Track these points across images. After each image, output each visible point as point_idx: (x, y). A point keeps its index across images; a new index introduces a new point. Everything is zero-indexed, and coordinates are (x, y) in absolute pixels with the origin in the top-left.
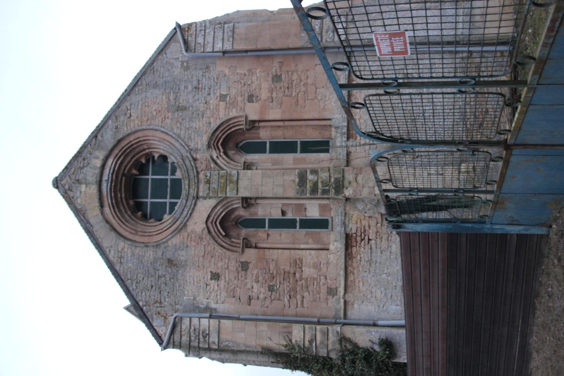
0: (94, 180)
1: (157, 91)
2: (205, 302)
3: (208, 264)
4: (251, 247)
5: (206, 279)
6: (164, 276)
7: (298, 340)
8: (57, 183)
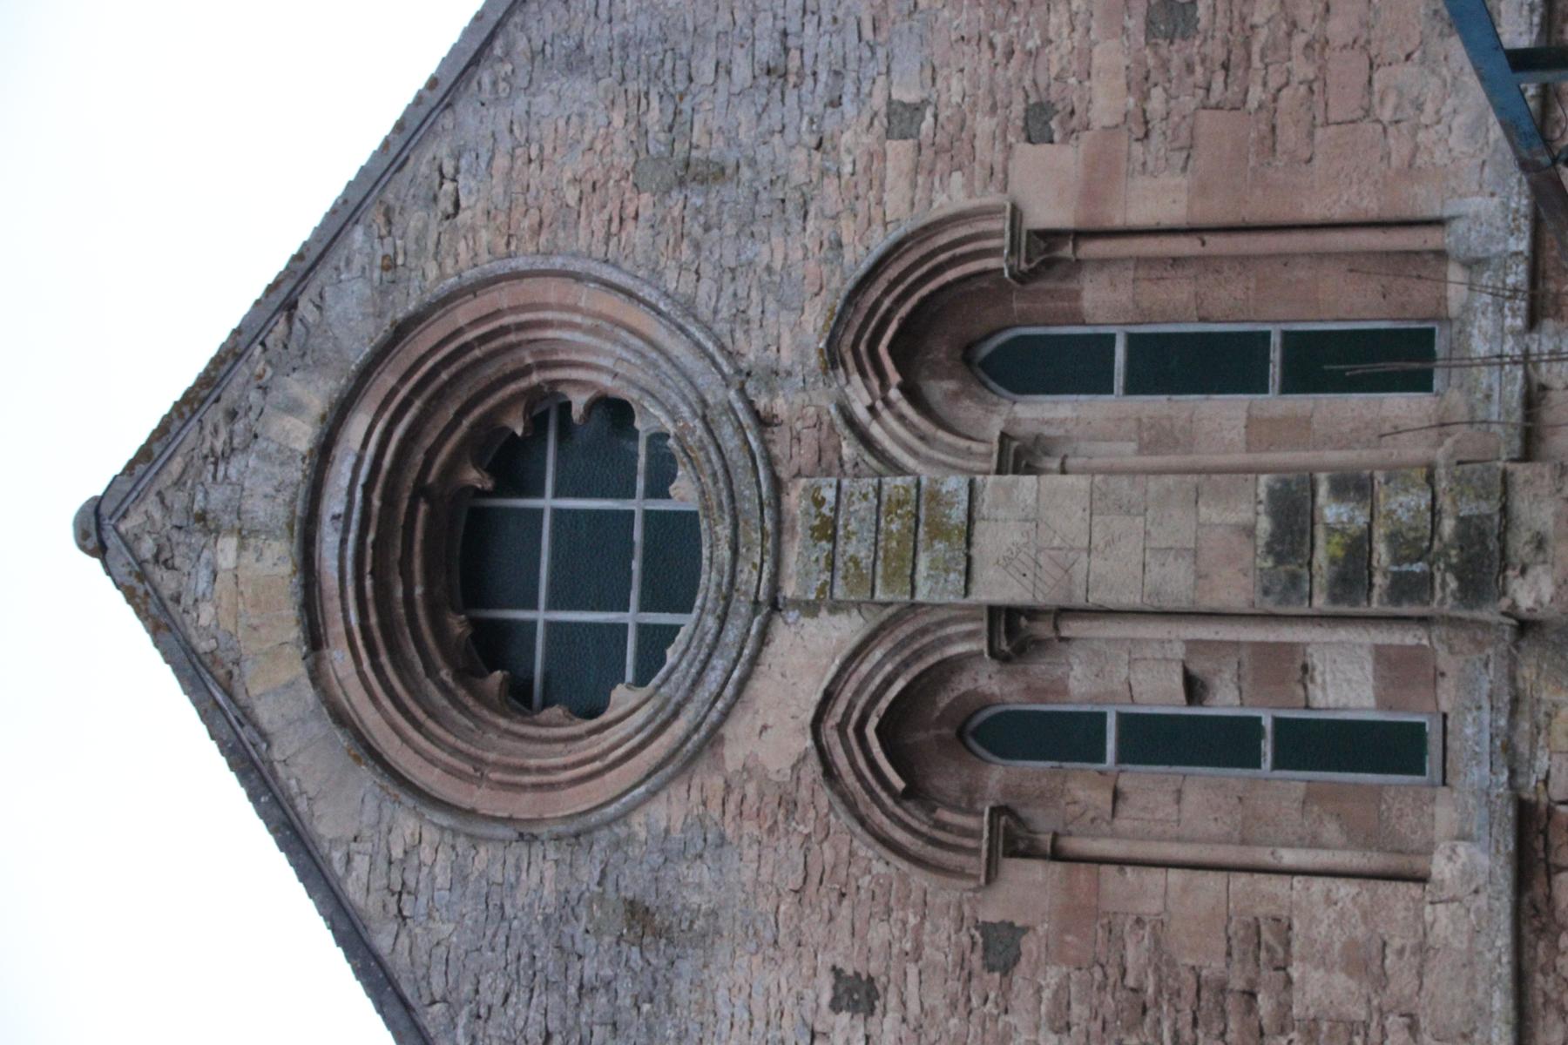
1: (581, 89)
3: (820, 933)
4: (1031, 853)
5: (809, 1003)
8: (97, 529)
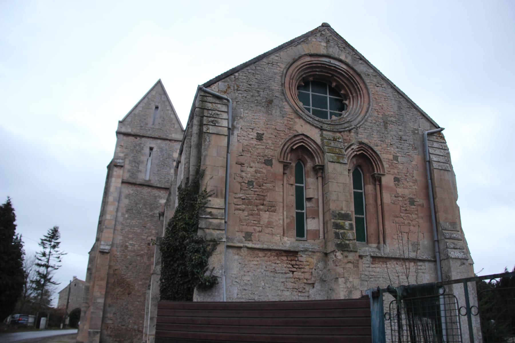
0: (331, 53)
1: (396, 109)
2: (239, 126)
3: (269, 132)
4: (284, 169)
5: (258, 129)
6: (259, 96)
7: (211, 202)
8: (325, 26)
